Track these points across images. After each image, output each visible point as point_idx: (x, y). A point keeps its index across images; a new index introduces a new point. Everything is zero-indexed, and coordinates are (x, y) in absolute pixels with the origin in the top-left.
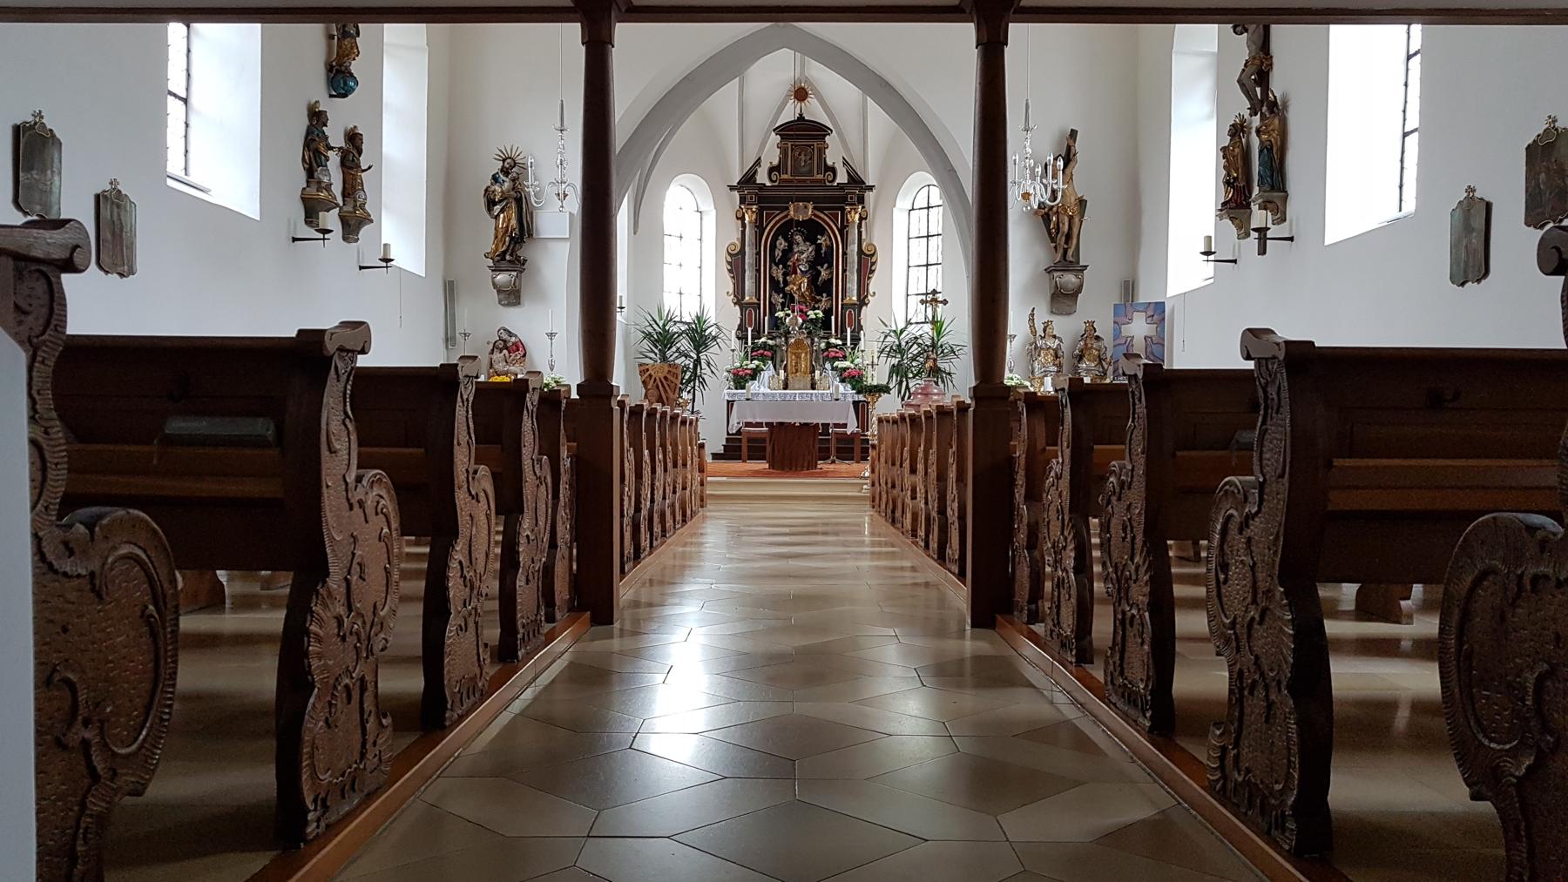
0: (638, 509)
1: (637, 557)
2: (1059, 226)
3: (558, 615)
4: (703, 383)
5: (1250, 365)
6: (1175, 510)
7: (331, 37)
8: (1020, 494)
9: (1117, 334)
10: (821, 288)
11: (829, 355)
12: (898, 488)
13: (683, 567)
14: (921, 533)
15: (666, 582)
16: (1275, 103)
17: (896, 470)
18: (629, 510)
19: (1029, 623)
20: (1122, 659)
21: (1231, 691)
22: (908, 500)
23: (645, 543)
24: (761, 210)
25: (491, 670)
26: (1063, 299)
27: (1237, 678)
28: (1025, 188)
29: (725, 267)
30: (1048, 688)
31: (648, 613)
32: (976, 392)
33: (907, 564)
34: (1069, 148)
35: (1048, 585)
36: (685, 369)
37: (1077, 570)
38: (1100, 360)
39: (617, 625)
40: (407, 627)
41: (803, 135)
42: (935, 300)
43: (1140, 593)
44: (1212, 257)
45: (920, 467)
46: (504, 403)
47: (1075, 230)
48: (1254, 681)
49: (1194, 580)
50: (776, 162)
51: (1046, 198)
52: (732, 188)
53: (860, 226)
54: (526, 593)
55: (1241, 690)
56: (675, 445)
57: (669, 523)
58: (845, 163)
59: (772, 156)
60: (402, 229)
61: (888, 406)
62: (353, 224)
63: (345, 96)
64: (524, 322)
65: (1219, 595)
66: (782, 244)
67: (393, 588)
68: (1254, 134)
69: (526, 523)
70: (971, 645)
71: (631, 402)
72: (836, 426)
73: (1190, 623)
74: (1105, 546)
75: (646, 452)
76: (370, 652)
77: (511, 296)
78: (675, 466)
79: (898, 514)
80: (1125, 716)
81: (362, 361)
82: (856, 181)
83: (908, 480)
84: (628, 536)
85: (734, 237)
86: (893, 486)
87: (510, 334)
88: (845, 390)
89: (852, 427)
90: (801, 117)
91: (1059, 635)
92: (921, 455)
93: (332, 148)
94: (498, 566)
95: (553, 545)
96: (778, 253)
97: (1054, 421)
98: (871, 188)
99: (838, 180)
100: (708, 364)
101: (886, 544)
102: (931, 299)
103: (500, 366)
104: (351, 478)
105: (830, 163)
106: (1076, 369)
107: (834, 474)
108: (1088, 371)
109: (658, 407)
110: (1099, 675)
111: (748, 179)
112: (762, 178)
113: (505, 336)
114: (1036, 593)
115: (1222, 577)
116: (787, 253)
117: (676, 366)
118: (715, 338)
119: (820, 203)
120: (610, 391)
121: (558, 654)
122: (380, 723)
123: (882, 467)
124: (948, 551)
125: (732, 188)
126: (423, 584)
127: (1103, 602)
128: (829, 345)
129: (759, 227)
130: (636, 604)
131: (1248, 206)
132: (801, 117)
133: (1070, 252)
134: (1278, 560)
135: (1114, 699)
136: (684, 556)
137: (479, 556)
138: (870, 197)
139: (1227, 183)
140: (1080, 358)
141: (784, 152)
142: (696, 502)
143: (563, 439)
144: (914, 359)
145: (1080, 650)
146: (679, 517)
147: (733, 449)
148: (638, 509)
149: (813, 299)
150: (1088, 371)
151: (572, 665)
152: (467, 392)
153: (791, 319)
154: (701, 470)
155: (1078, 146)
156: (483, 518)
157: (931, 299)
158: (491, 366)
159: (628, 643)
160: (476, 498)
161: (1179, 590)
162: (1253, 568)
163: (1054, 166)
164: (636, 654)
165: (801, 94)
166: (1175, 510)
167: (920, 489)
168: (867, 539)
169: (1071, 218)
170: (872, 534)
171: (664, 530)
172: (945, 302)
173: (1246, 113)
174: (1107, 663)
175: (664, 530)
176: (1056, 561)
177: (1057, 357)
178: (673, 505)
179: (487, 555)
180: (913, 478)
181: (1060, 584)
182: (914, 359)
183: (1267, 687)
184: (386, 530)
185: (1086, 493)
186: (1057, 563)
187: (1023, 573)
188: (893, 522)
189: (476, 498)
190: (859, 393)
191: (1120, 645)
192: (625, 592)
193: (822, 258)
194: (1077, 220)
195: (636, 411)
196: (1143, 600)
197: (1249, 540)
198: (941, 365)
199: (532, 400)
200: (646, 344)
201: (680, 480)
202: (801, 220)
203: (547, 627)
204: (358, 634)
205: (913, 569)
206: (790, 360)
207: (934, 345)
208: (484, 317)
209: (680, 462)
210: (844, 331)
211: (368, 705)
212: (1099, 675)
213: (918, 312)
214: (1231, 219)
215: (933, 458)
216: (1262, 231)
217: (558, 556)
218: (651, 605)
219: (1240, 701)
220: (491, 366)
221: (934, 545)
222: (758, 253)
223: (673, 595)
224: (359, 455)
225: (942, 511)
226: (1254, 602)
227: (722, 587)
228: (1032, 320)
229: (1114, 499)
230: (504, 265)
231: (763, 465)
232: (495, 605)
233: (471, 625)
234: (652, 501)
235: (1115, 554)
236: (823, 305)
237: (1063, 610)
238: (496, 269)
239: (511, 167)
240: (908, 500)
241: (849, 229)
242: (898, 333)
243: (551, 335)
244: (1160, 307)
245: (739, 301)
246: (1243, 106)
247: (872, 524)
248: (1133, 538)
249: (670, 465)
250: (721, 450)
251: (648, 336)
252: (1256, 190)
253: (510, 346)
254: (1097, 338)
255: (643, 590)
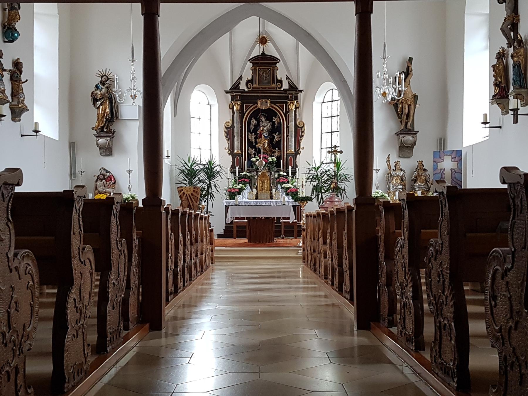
0: (176, 266)
1: (176, 293)
2: (403, 110)
3: (131, 326)
4: (212, 196)
5: (506, 186)
6: (467, 266)
7: (5, 9)
8: (381, 256)
9: (435, 168)
10: (275, 145)
11: (280, 181)
12: (317, 253)
13: (202, 297)
14: (330, 277)
15: (192, 305)
16: (521, 41)
17: (316, 243)
18: (171, 266)
19: (388, 327)
20: (440, 348)
21: (500, 367)
22: (322, 259)
23: (180, 284)
24: (242, 104)
25: (91, 359)
26: (405, 149)
27: (503, 360)
28: (383, 90)
29: (223, 135)
30: (401, 365)
31: (181, 323)
32: (357, 201)
33: (322, 293)
34: (408, 67)
35: (398, 305)
36: (203, 189)
37: (414, 298)
38: (426, 182)
39: (164, 331)
40: (44, 334)
41: (264, 63)
42: (336, 151)
43: (448, 312)
44: (487, 125)
45: (328, 241)
46: (100, 212)
47: (412, 112)
48: (513, 363)
49: (481, 303)
50: (250, 78)
51: (395, 96)
52: (227, 92)
53: (295, 112)
54: (112, 314)
55: (506, 367)
56: (196, 230)
57: (194, 272)
58: (287, 78)
59: (248, 75)
60: (45, 114)
61: (312, 208)
62: (17, 112)
63: (12, 41)
64: (114, 165)
65: (492, 313)
66: (254, 122)
67: (35, 314)
68: (510, 58)
69: (113, 276)
70: (357, 339)
71: (172, 208)
72: (284, 218)
73: (477, 327)
74: (428, 284)
75: (181, 235)
76: (21, 351)
77: (107, 151)
78: (197, 242)
79: (317, 266)
80: (443, 381)
81: (17, 189)
82: (293, 87)
83: (322, 248)
84: (170, 280)
85: (229, 119)
86: (314, 251)
87: (107, 171)
88: (288, 199)
89: (292, 219)
90: (263, 53)
91: (405, 334)
92: (328, 234)
93: (5, 70)
94: (96, 299)
95: (128, 287)
96: (252, 127)
97: (399, 217)
98: (301, 91)
99: (284, 87)
100: (215, 186)
101: (311, 283)
102: (334, 150)
103: (101, 189)
104: (11, 255)
105: (279, 78)
106: (413, 188)
107: (283, 245)
108: (420, 188)
109: (187, 210)
110: (428, 357)
111: (236, 87)
112: (243, 86)
113: (104, 173)
114: (392, 310)
115: (493, 303)
116: (257, 126)
117: (198, 188)
118: (218, 173)
119: (275, 100)
120: (160, 203)
121: (132, 346)
122: (27, 391)
123: (308, 241)
124: (344, 287)
125: (227, 92)
126: (53, 310)
127: (428, 315)
128: (280, 176)
129: (242, 113)
130: (175, 318)
131: (507, 97)
132: (263, 53)
133: (409, 124)
134: (524, 294)
135: (436, 371)
136: (202, 291)
137: (86, 296)
138: (301, 96)
139: (496, 85)
140: (415, 181)
141: (254, 72)
142: (208, 261)
143: (134, 229)
144: (325, 183)
145: (416, 342)
146: (199, 269)
147: (231, 231)
148: (176, 266)
149: (271, 151)
150: (420, 188)
151: (138, 355)
152: (79, 205)
153: (259, 162)
154: (211, 243)
155: (413, 66)
156: (88, 274)
157: (334, 150)
158: (96, 189)
159: (171, 340)
160: (84, 263)
161: (471, 309)
162: (510, 298)
163: (400, 77)
164: (175, 347)
165: (263, 41)
166: (467, 266)
167: (328, 252)
168: (301, 280)
169: (409, 106)
170: (304, 277)
171: (191, 277)
172: (341, 152)
173: (506, 47)
174: (432, 350)
175: (191, 277)
176: (402, 293)
177: (402, 180)
178: (196, 263)
179: (90, 294)
180: (325, 247)
181: (404, 306)
182: (325, 183)
183: (520, 366)
184: (31, 283)
185: (417, 256)
186: (403, 294)
187: (385, 299)
188: (315, 271)
189: (84, 263)
190: (295, 201)
191: (438, 341)
192: (168, 312)
193: (276, 129)
194: (412, 106)
195: (175, 213)
196: (450, 315)
197: (507, 283)
198: (340, 185)
199: (116, 209)
200: (182, 176)
201: (200, 250)
202: (264, 108)
203: (124, 333)
204: (14, 342)
205: (326, 296)
206: (259, 184)
207: (335, 175)
208: (92, 162)
209: (199, 240)
210: (287, 168)
211: (20, 382)
212: (428, 357)
213: (327, 157)
214: (498, 104)
215: (335, 236)
216: (515, 111)
217: (131, 293)
218: (183, 319)
219: (506, 373)
220: (96, 189)
221: (336, 283)
222: (241, 127)
223: (195, 313)
224: (16, 240)
225: (340, 265)
226: (511, 317)
227: (222, 308)
228: (388, 160)
229: (433, 259)
230: (102, 134)
231: (245, 240)
232: (95, 321)
233: (80, 333)
234: (184, 261)
235: (434, 290)
236: (276, 154)
237: (407, 321)
238: (98, 136)
239: (106, 81)
240: (322, 259)
241: (290, 113)
242: (317, 169)
243: (129, 172)
244: (459, 153)
245: (231, 153)
246: (503, 42)
247: (303, 272)
248: (444, 281)
249: (194, 241)
250: (222, 232)
251: (183, 171)
252: (512, 88)
253: (106, 178)
254: (425, 170)
255: (179, 311)
